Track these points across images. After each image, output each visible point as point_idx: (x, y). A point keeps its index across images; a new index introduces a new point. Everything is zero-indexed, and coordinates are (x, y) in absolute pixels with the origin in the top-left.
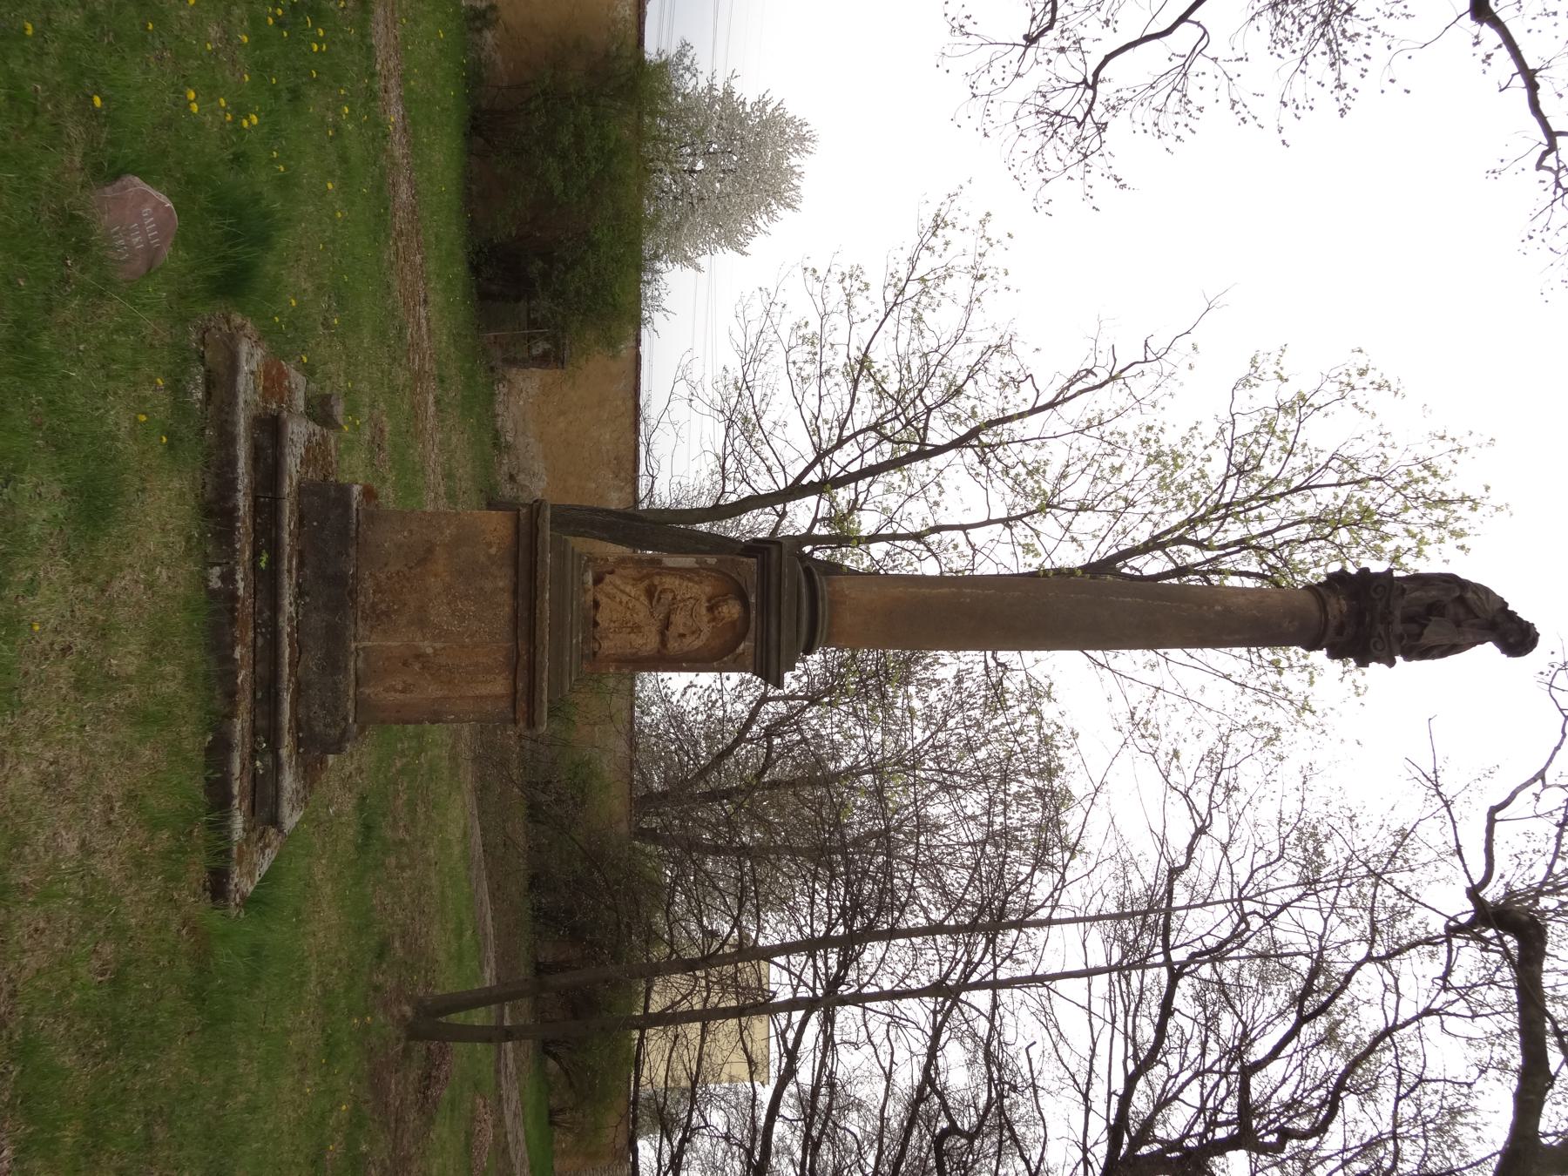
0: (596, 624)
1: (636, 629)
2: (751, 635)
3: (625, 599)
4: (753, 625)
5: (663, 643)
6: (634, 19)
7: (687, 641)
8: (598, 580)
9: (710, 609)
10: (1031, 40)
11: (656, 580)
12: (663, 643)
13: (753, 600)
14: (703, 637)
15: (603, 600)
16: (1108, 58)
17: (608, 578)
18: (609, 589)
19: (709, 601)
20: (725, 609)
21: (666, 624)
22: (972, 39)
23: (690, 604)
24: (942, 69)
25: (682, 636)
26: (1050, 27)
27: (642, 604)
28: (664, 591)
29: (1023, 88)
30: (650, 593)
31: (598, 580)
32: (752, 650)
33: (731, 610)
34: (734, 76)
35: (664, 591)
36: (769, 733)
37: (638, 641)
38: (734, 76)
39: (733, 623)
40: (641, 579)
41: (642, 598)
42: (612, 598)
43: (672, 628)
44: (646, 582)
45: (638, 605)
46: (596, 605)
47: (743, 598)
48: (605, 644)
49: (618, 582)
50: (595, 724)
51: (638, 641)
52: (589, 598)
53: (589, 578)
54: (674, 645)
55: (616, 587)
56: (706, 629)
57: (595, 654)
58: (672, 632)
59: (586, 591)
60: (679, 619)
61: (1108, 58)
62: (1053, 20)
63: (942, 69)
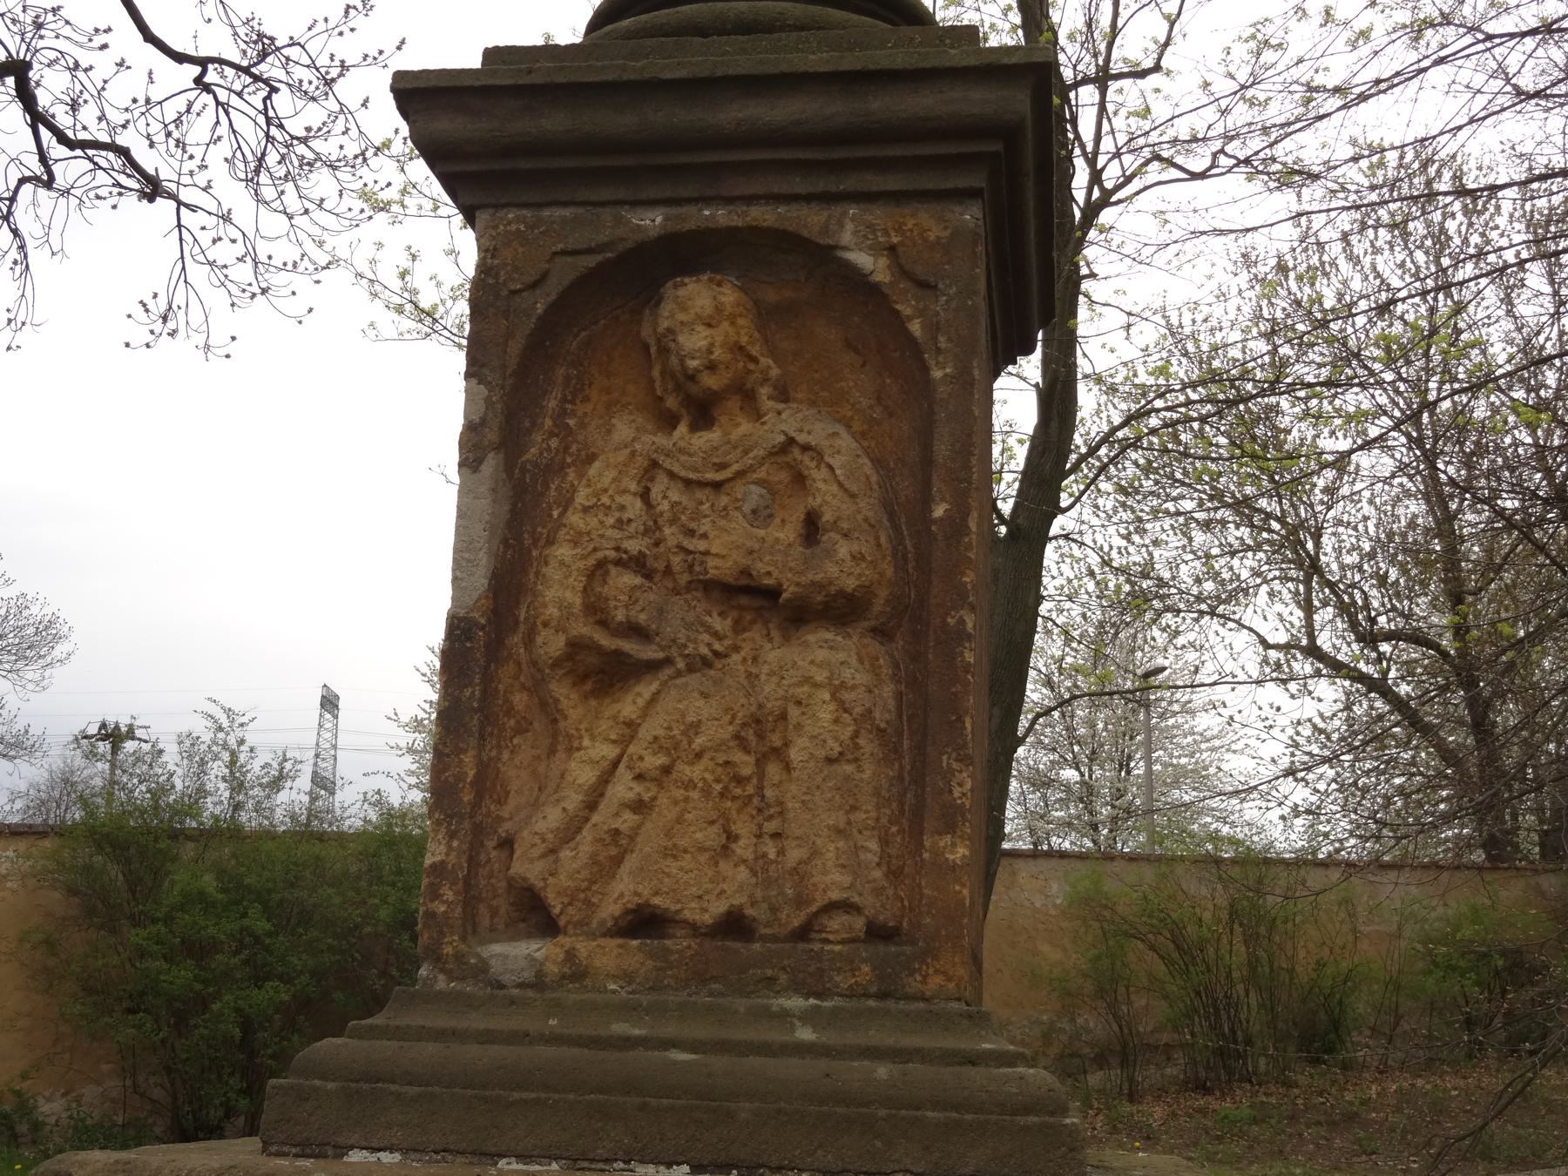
0: (734, 926)
1: (764, 734)
2: (810, 220)
3: (623, 788)
4: (764, 215)
5: (840, 610)
6: (22, 845)
7: (826, 496)
8: (534, 914)
9: (703, 412)
10: (152, 189)
11: (552, 644)
12: (840, 610)
13: (652, 221)
14: (817, 430)
15: (624, 890)
16: (149, 37)
17: (528, 868)
18: (574, 860)
19: (668, 422)
20: (694, 341)
21: (752, 598)
22: (179, 299)
23: (666, 494)
24: (231, 348)
25: (812, 528)
26: (124, 152)
27: (659, 709)
28: (596, 610)
29: (234, 195)
30: (607, 673)
31: (534, 914)
32: (877, 215)
33: (701, 318)
34: (394, 718)
35: (596, 610)
36: (1369, 638)
37: (819, 727)
38: (394, 718)
39: (767, 316)
40: (551, 712)
41: (628, 707)
42: (618, 845)
43: (767, 570)
44: (563, 692)
45: (652, 728)
46: (644, 923)
47: (644, 272)
48: (832, 882)
49: (551, 818)
50: (1355, 930)
51: (819, 727)
52: (607, 956)
53: (515, 955)
54: (845, 564)
55: (570, 832)
56: (783, 422)
57: (878, 933)
58: (784, 566)
59: (576, 973)
60: (727, 543)
61: (149, 37)
62: (113, 147)
63: (231, 348)
